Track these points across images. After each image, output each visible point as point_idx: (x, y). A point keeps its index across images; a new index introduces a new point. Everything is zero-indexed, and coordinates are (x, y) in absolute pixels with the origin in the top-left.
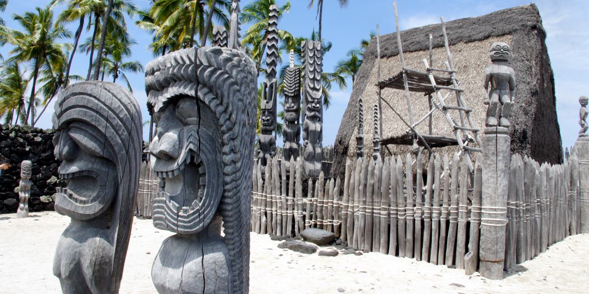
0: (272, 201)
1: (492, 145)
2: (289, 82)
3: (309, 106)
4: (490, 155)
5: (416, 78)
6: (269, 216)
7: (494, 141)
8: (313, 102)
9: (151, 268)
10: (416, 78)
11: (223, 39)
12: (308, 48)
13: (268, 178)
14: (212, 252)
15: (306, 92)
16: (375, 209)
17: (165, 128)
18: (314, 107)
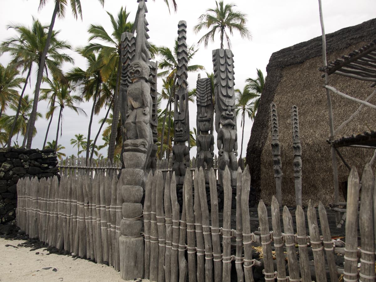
2: (201, 92)
3: (224, 113)
6: (190, 258)
8: (226, 110)
9: (13, 245)
11: (132, 45)
12: (219, 55)
13: (189, 201)
15: (219, 99)
17: (105, 219)
18: (228, 114)
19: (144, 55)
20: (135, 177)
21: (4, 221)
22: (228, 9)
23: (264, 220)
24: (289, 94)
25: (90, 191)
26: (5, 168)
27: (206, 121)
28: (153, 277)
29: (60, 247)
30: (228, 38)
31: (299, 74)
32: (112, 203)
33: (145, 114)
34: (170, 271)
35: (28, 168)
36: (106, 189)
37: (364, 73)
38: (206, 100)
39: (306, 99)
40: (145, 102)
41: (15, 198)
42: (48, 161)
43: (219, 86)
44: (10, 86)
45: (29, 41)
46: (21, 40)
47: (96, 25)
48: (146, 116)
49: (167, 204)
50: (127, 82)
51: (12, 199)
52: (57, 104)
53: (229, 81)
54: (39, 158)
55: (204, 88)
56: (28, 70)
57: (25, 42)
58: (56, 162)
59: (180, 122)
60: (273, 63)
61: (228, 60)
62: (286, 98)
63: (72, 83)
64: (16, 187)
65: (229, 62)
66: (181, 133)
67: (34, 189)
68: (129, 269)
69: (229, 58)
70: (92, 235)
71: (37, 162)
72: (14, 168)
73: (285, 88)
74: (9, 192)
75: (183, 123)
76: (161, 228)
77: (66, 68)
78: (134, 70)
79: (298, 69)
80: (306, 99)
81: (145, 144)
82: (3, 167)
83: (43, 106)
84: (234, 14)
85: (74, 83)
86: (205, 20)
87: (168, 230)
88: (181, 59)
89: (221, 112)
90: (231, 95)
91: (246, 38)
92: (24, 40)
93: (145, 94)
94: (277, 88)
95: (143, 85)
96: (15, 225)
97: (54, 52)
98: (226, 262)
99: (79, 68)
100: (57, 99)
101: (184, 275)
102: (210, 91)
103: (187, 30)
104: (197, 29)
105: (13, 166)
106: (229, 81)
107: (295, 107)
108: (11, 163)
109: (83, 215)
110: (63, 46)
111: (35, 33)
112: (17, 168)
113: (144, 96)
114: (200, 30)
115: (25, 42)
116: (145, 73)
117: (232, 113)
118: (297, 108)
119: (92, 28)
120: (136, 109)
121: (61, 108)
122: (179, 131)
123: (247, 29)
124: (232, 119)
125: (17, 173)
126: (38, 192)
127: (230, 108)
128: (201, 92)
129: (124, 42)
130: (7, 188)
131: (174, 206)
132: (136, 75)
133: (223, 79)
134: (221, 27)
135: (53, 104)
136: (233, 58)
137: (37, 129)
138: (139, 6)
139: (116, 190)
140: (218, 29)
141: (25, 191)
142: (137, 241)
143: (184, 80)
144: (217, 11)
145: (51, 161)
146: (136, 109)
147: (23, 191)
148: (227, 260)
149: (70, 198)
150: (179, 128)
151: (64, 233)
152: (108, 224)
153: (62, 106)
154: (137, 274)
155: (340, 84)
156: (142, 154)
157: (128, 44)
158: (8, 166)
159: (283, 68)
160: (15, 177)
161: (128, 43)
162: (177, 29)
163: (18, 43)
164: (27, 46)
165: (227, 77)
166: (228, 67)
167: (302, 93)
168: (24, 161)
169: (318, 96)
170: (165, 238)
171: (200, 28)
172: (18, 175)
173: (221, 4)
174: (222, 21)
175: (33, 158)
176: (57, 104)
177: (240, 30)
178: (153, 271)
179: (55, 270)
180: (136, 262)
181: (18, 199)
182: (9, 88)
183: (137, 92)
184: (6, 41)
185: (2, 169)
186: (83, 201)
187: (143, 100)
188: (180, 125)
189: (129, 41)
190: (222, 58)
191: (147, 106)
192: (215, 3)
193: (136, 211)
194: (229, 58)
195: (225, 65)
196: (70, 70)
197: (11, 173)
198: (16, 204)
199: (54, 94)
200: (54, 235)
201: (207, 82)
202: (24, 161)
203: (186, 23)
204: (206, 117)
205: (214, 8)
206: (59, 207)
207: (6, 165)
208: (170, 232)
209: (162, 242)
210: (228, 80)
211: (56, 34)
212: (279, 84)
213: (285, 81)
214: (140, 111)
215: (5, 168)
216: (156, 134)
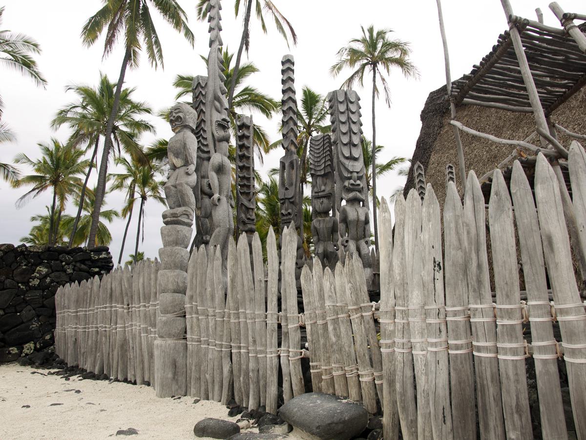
0: (256, 356)
2: (316, 155)
3: (346, 183)
5: (561, 58)
8: (350, 178)
10: (561, 58)
12: (337, 100)
15: (339, 162)
16: (505, 351)
18: (352, 184)
19: (217, 104)
20: (173, 257)
21: (38, 347)
22: (380, 36)
23: (307, 291)
24: (451, 151)
25: (130, 288)
26: (40, 274)
27: (324, 197)
28: (195, 392)
29: (99, 372)
30: (383, 80)
31: (467, 119)
32: (152, 299)
33: (188, 174)
34: (214, 381)
35: (72, 274)
36: (146, 281)
37: (513, 100)
38: (323, 166)
39: (475, 155)
40: (189, 158)
41: (54, 316)
42: (99, 264)
43: (339, 145)
44: (70, 173)
45: (93, 107)
46: (84, 105)
47: (185, 75)
48: (190, 177)
49: (209, 290)
51: (49, 317)
52: (137, 196)
53: (352, 134)
54: (88, 260)
55: (319, 149)
56: (93, 147)
57: (88, 108)
58: (111, 265)
59: (287, 201)
60: (430, 108)
61: (350, 106)
62: (447, 157)
63: (155, 162)
64: (54, 298)
65: (353, 108)
66: (289, 217)
67: (73, 297)
68: (164, 383)
69: (352, 103)
70: (133, 348)
71: (85, 265)
72: (53, 274)
73: (446, 143)
74: (46, 307)
75: (292, 203)
76: (203, 323)
77: (146, 141)
78: (174, 117)
79: (466, 113)
80: (475, 155)
81: (188, 213)
82: (37, 273)
83: (115, 200)
84: (390, 43)
85: (158, 161)
86: (346, 57)
87: (211, 324)
88: (287, 109)
89: (344, 182)
91: (411, 78)
92: (87, 105)
93: (188, 147)
94: (435, 143)
95: (185, 136)
96: (53, 353)
97: (129, 119)
98: (271, 356)
99: (164, 140)
100: (137, 189)
101: (228, 383)
102: (329, 153)
103: (295, 68)
104: (336, 69)
105: (50, 271)
107: (450, 167)
108: (48, 266)
109: (122, 322)
110: (141, 110)
111: (103, 96)
112: (57, 274)
113: (188, 150)
114: (341, 72)
115: (88, 108)
116: (189, 120)
117: (358, 182)
118: (454, 168)
119: (179, 81)
120: (178, 168)
121: (142, 200)
122: (287, 215)
123: (412, 64)
124: (360, 191)
125: (57, 280)
126: (77, 301)
127: (355, 174)
128: (316, 155)
129: (196, 89)
130: (43, 301)
131: (217, 291)
132: (177, 123)
133: (344, 134)
134: (371, 64)
135: (132, 195)
136: (359, 102)
137: (112, 235)
138: (210, 39)
139: (156, 279)
140: (368, 68)
141: (64, 304)
144: (364, 41)
145: (104, 264)
146: (178, 168)
147: (63, 304)
148: (272, 354)
149: (111, 302)
150: (286, 210)
151: (104, 351)
152: (149, 328)
153: (144, 198)
154: (177, 390)
155: (525, 128)
156: (185, 227)
157: (201, 92)
158: (44, 270)
159: (444, 113)
160: (54, 286)
161: (201, 90)
162: (281, 67)
163: (79, 110)
164: (91, 114)
165: (350, 130)
166: (352, 116)
167: (470, 147)
168: (67, 264)
169: (492, 150)
170: (208, 336)
171: (339, 69)
172: (57, 283)
173: (371, 30)
174: (373, 55)
175: (79, 259)
176: (137, 196)
177: (402, 67)
178: (195, 384)
179: (78, 392)
180: (175, 374)
181: (57, 316)
182: (71, 176)
183: (178, 145)
184: (63, 108)
185: (35, 276)
186: (123, 303)
187: (186, 155)
188: (288, 205)
189: (202, 87)
190: (341, 103)
191: (192, 163)
192: (361, 29)
193: (176, 303)
194: (352, 103)
195: (346, 112)
196: (152, 143)
197: (48, 280)
198: (55, 323)
199: (133, 180)
200: (93, 356)
201: (324, 141)
202: (67, 264)
204: (324, 191)
205: (360, 38)
206: (99, 317)
207: (41, 269)
208: (214, 327)
210: (352, 134)
211: (129, 93)
212: (438, 138)
213: (446, 132)
214: (183, 169)
215: (40, 274)
216: (253, 220)
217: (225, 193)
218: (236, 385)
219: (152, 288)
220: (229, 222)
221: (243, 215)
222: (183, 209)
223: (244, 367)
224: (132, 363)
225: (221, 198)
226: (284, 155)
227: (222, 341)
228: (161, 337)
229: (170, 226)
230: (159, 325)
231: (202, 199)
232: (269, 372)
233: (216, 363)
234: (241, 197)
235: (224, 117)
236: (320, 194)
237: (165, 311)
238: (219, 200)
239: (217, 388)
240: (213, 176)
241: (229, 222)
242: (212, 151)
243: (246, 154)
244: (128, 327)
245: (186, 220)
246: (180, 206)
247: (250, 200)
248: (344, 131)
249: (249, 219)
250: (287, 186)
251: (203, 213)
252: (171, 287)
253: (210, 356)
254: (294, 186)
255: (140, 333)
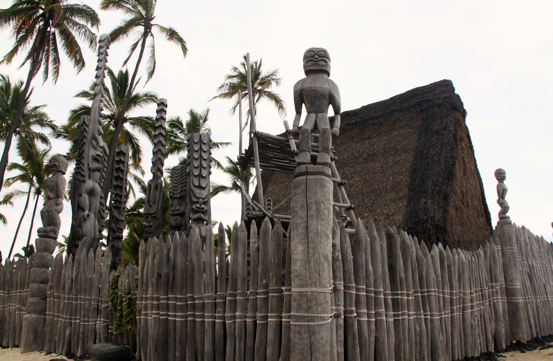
1: (300, 193)
4: (297, 210)
7: (303, 187)
8: (197, 203)
14: (61, 206)
15: (190, 189)
18: (198, 208)
19: (94, 142)
38: (180, 190)
50: (80, 170)
53: (202, 169)
59: (150, 216)
61: (203, 146)
90: (204, 186)
103: (167, 110)
106: (202, 169)
117: (203, 206)
122: (149, 227)
127: (201, 200)
133: (196, 168)
142: (38, 317)
143: (158, 168)
157: (85, 129)
165: (201, 165)
180: (35, 338)
186: (5, 290)
190: (196, 143)
203: (166, 102)
204: (178, 210)
209: (231, 318)
217: (94, 211)
218: (73, 343)
219: (27, 280)
220: (95, 232)
221: (114, 225)
222: (51, 227)
223: (77, 331)
224: (7, 334)
225: (90, 214)
226: (152, 178)
227: (67, 315)
228: (28, 313)
229: (42, 238)
230: (28, 304)
231: (78, 212)
232: (90, 333)
233: (62, 330)
234: (114, 210)
235: (98, 153)
236: (175, 212)
237: (33, 296)
238: (88, 215)
239: (61, 345)
240: (86, 197)
241: (95, 232)
242: (87, 177)
243: (121, 176)
244: (7, 307)
245: (53, 235)
246: (50, 225)
247: (120, 213)
248: (196, 166)
249: (118, 228)
250: (151, 204)
251: (78, 223)
252: (38, 279)
253: (59, 325)
254: (156, 205)
255: (15, 311)
